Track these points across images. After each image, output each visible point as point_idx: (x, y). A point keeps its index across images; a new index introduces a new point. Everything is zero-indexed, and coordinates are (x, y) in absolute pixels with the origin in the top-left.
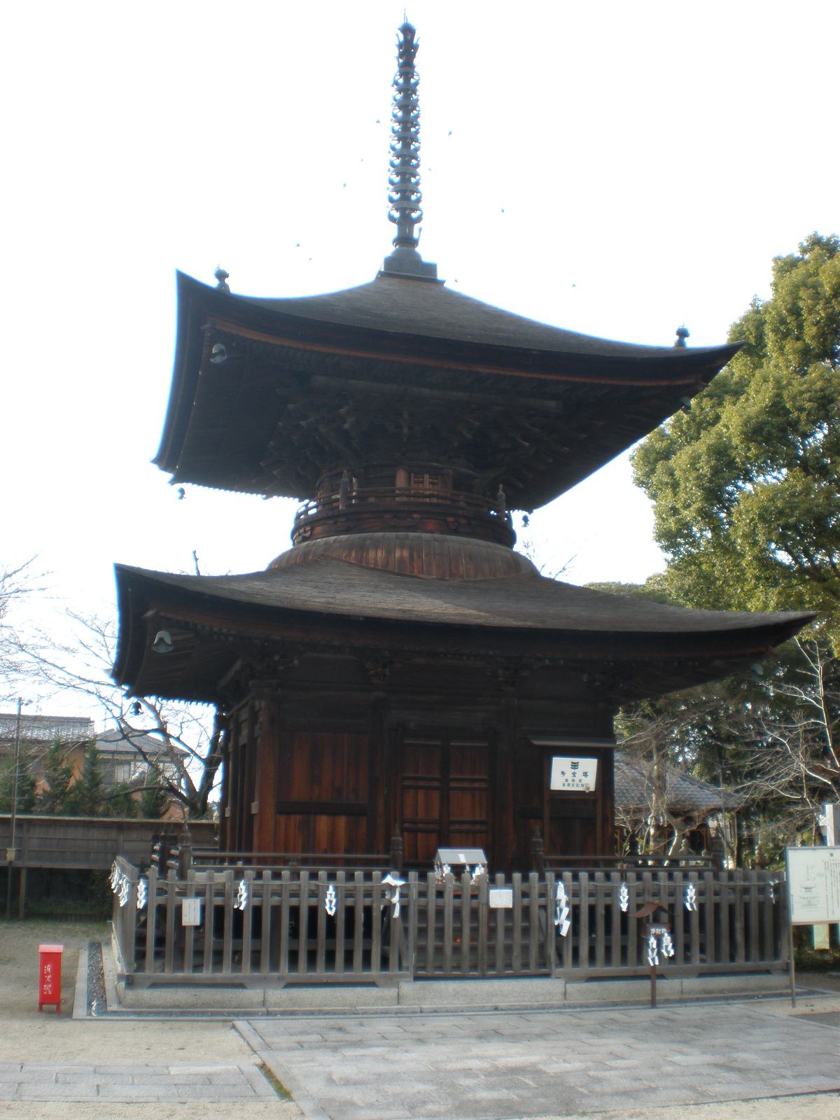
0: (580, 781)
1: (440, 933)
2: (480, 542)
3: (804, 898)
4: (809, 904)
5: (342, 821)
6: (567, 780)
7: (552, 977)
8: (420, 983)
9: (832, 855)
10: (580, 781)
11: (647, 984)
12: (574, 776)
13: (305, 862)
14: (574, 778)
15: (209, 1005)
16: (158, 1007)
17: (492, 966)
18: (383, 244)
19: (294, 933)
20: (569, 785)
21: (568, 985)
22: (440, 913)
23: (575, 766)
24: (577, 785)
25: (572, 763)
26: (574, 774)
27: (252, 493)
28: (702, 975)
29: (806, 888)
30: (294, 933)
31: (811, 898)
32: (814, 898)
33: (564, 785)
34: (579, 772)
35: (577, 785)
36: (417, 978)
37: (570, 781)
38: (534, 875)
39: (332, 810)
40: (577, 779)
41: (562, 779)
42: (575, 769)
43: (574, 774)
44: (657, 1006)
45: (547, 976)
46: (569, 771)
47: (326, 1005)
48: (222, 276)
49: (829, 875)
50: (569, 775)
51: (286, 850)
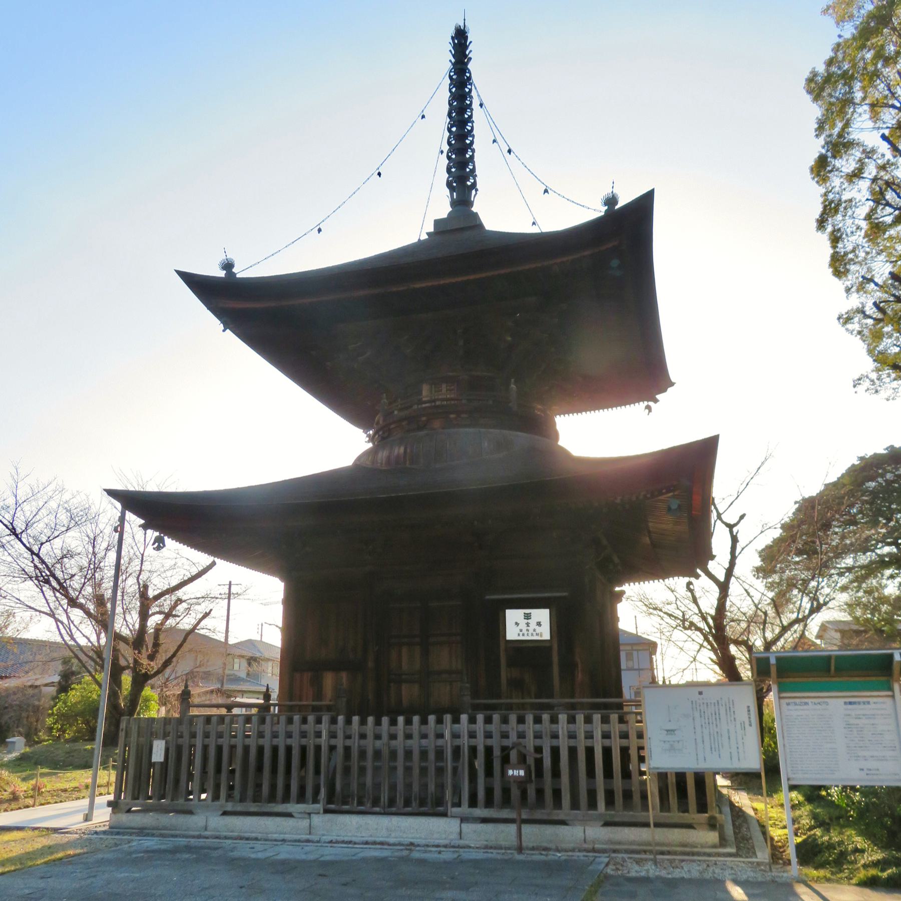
0: (534, 630)
1: (440, 771)
2: (467, 430)
3: (665, 742)
4: (672, 749)
5: (344, 676)
6: (521, 631)
7: (113, 815)
8: (329, 816)
9: (700, 693)
10: (534, 630)
11: (513, 828)
12: (528, 626)
13: (596, 707)
14: (528, 628)
15: (165, 828)
16: (133, 828)
17: (376, 802)
18: (442, 207)
19: (591, 773)
20: (523, 635)
21: (462, 825)
22: (440, 753)
23: (528, 617)
24: (532, 635)
25: (525, 613)
26: (528, 624)
27: (581, 412)
28: (607, 824)
29: (667, 731)
30: (591, 773)
31: (674, 741)
32: (678, 742)
33: (519, 635)
34: (533, 622)
35: (532, 635)
36: (326, 811)
37: (524, 631)
38: (385, 720)
39: (336, 666)
40: (531, 629)
41: (517, 629)
42: (528, 619)
43: (528, 624)
44: (523, 852)
45: (444, 815)
46: (523, 622)
47: (252, 832)
48: (228, 266)
49: (697, 714)
50: (522, 625)
51: (301, 700)
